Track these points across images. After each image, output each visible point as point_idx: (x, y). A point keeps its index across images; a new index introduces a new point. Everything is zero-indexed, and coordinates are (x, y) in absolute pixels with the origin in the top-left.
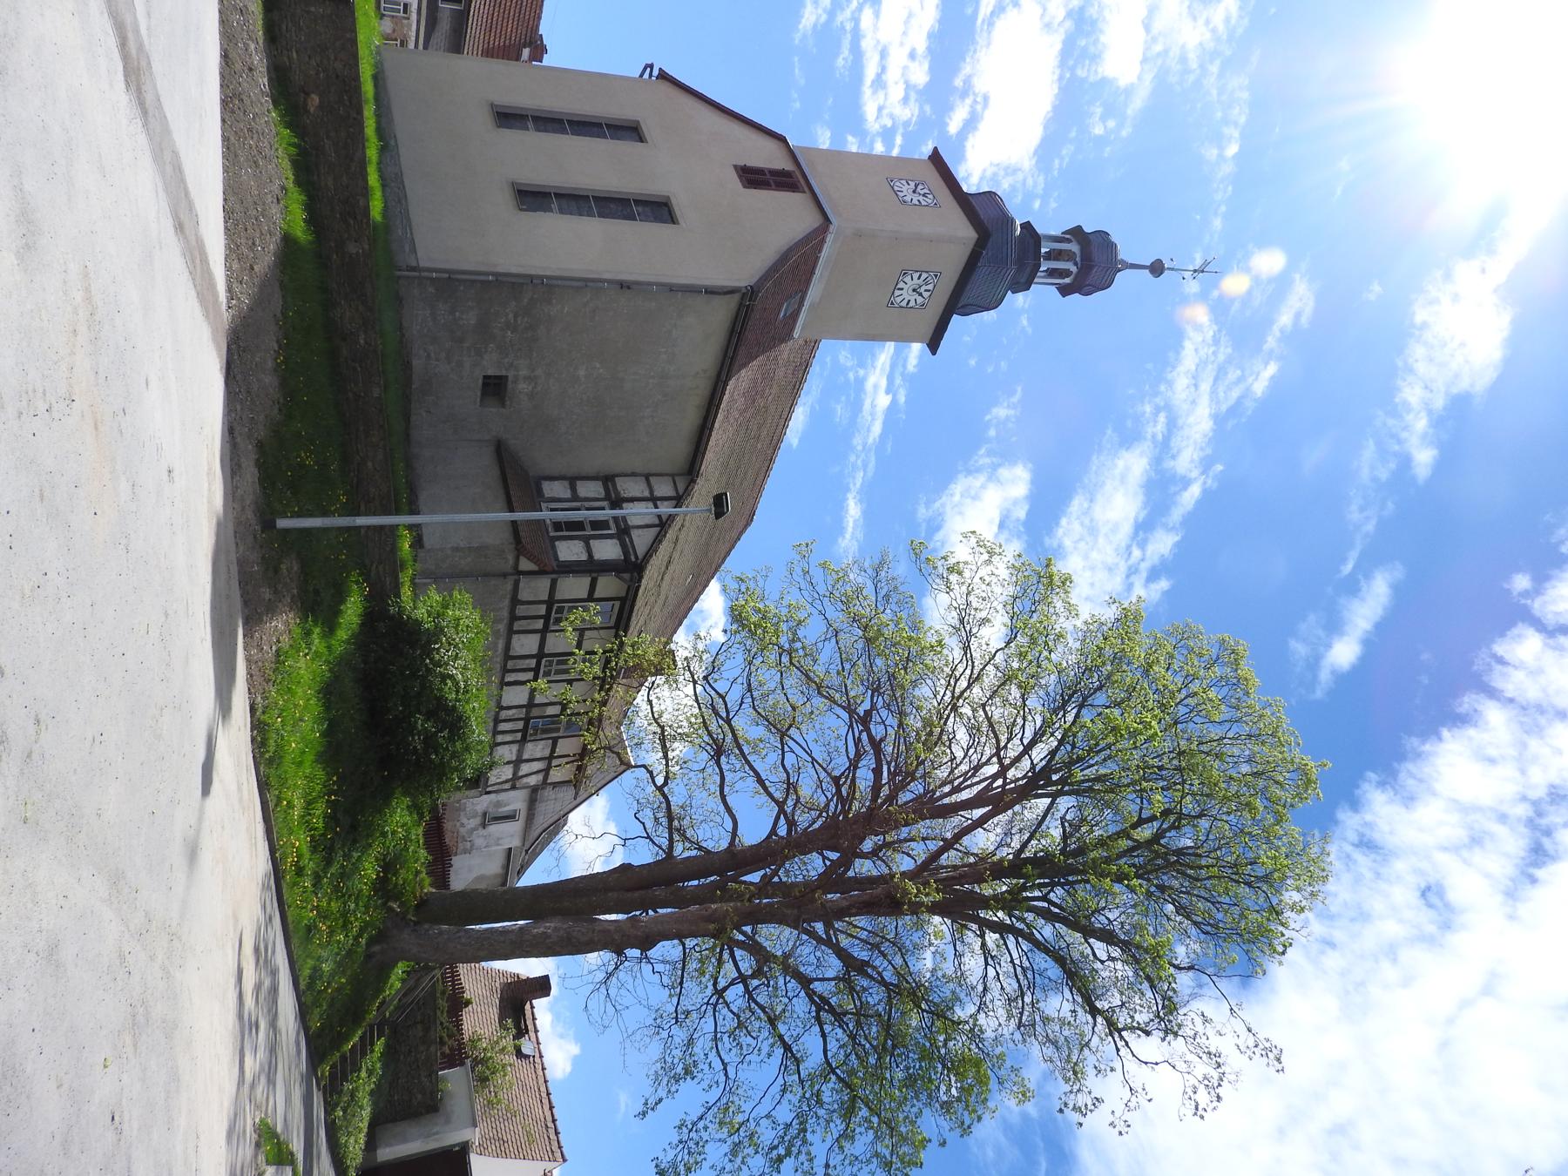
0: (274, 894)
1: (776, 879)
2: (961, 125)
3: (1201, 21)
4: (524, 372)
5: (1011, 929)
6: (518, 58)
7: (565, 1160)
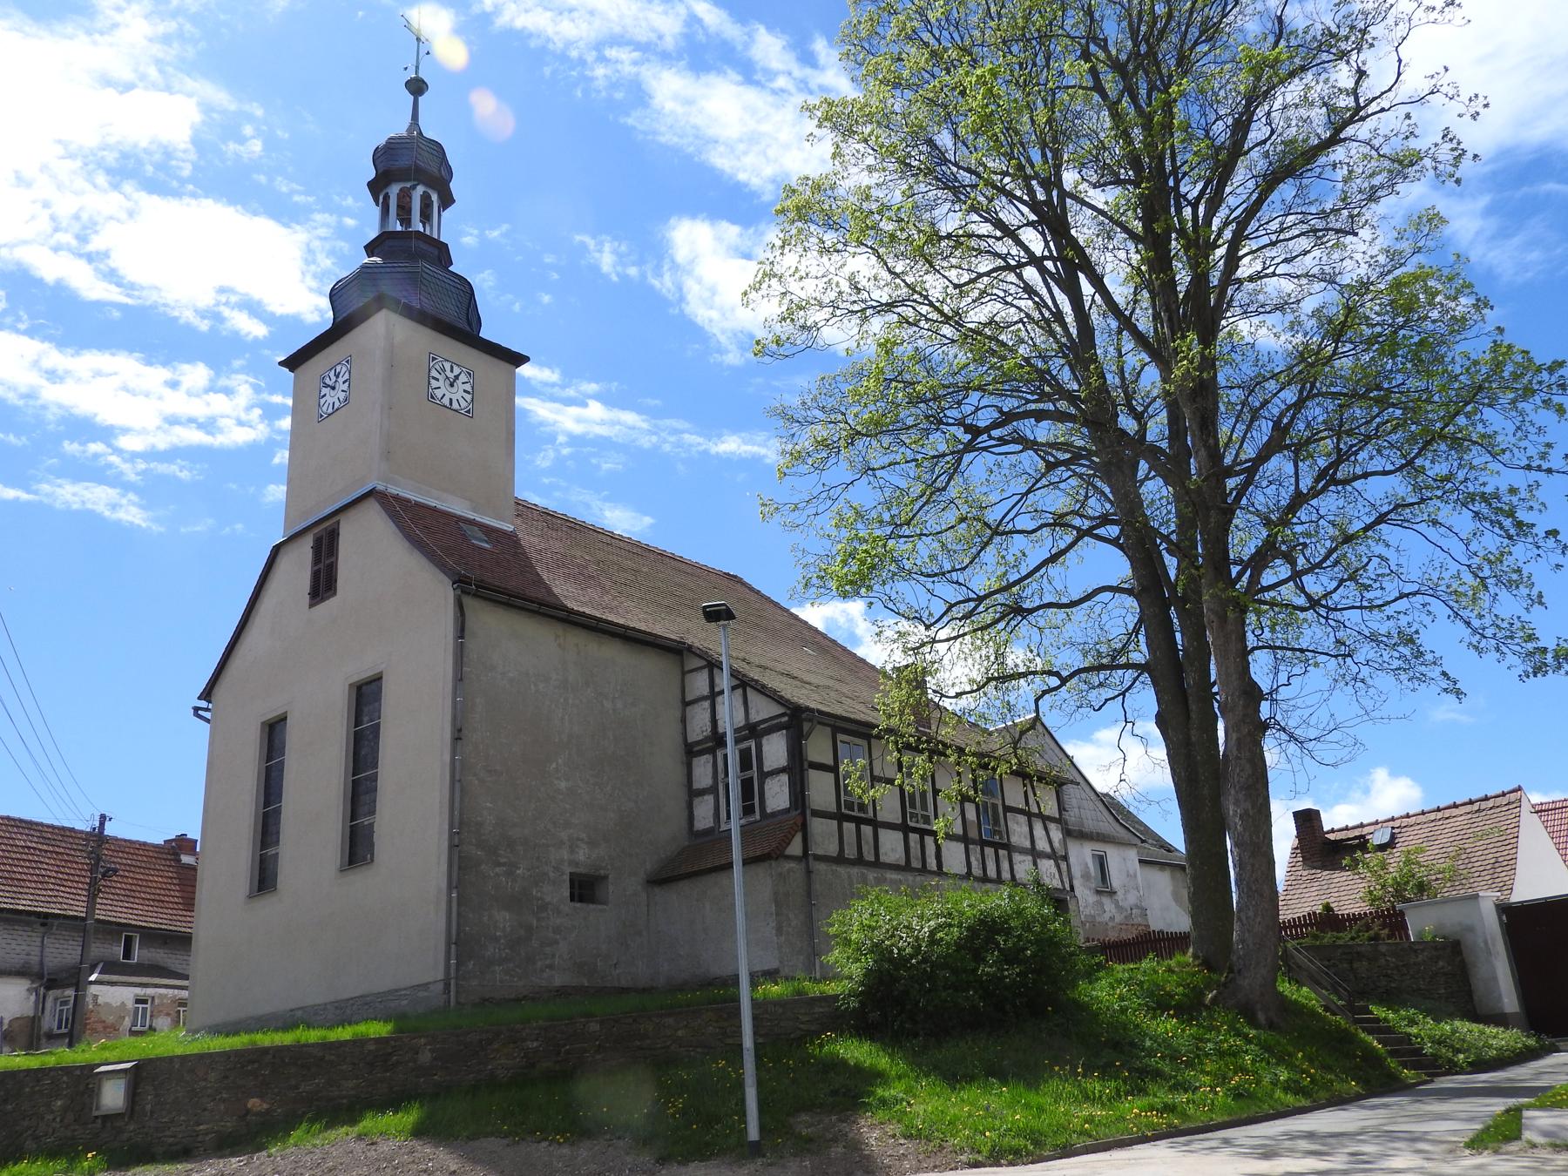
0: (1197, 1137)
1: (1174, 537)
2: (255, 321)
3: (118, 18)
4: (565, 854)
5: (1234, 245)
6: (193, 869)
7: (1520, 789)
